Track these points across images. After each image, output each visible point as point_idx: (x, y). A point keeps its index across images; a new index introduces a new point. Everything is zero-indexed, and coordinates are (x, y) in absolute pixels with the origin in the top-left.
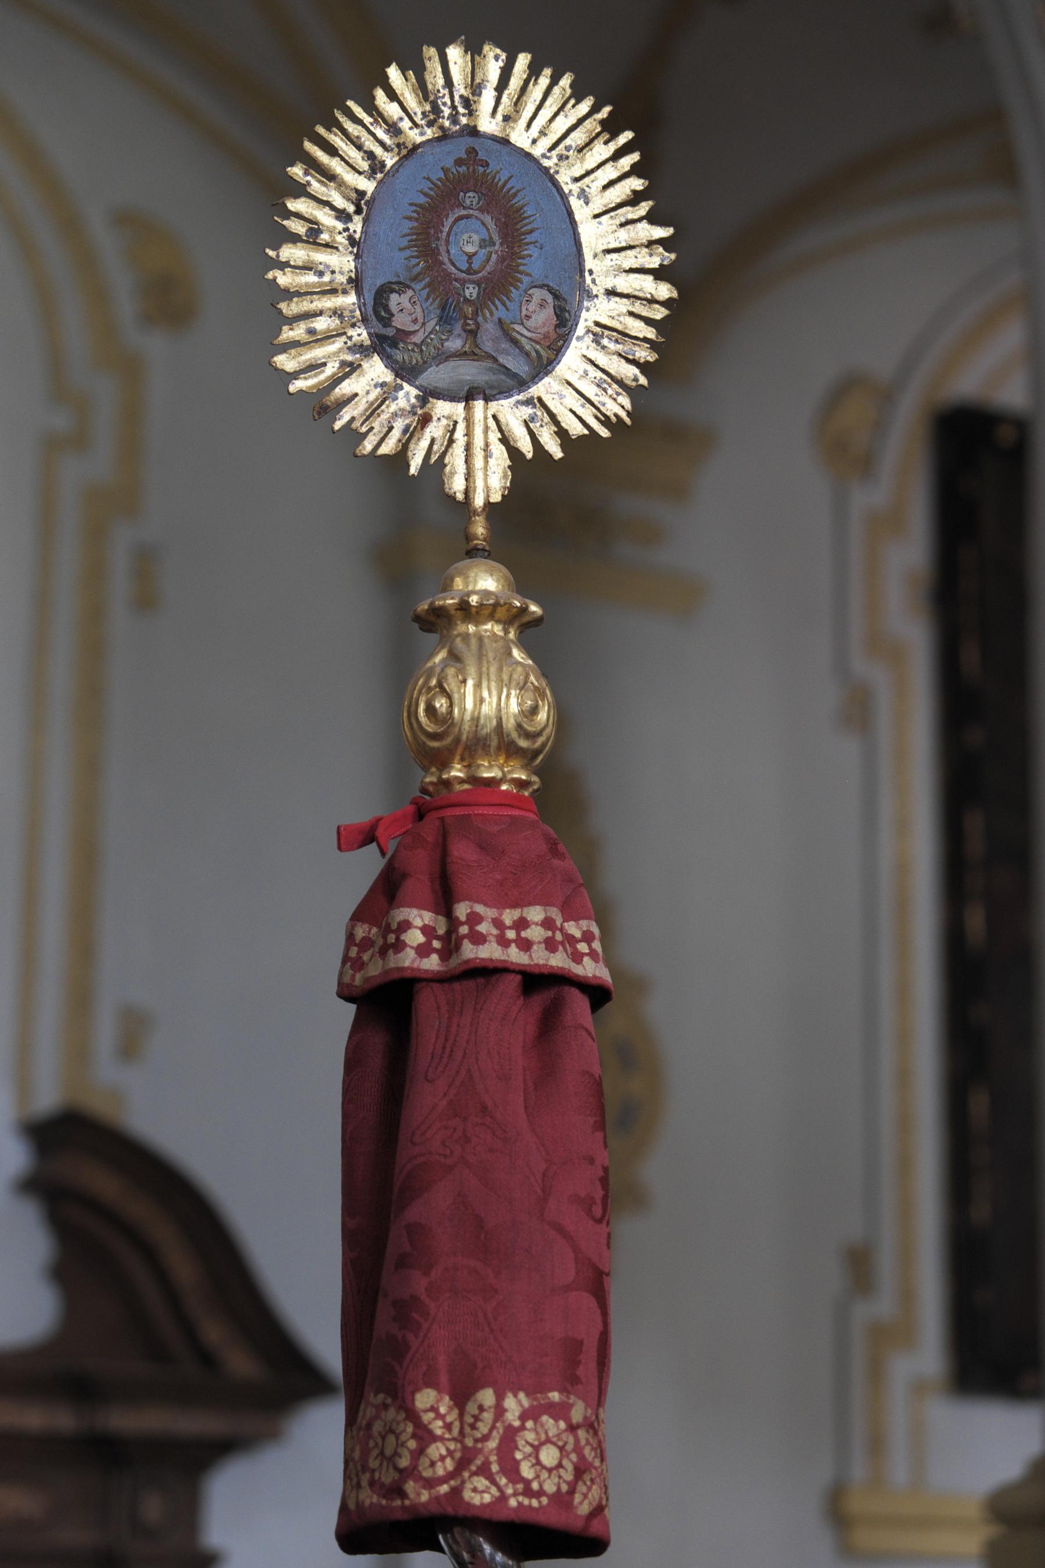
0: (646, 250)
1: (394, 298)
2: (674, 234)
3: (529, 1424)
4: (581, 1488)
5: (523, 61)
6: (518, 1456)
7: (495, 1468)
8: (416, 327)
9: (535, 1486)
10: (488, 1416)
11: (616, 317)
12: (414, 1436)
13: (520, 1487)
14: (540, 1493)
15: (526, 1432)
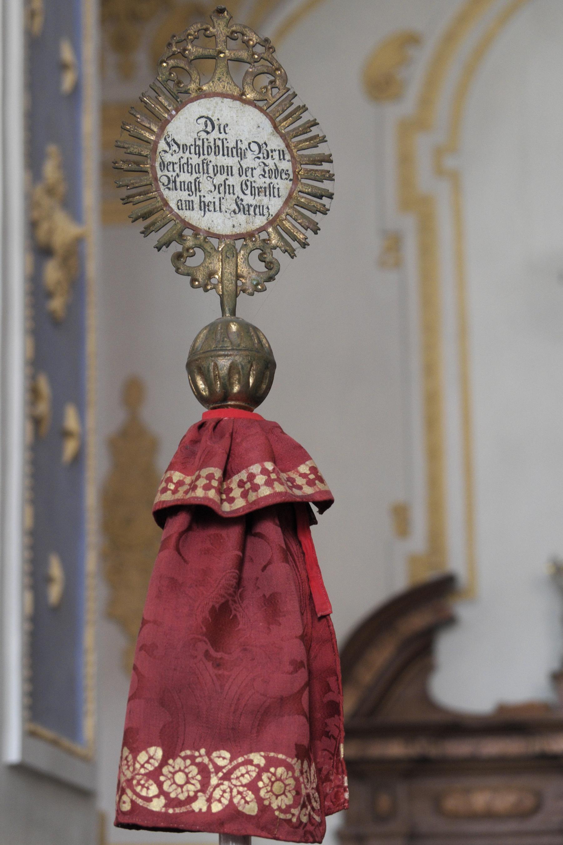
0: (154, 757)
6: (199, 777)
9: (188, 762)
11: (288, 777)
12: (259, 789)
14: (184, 758)
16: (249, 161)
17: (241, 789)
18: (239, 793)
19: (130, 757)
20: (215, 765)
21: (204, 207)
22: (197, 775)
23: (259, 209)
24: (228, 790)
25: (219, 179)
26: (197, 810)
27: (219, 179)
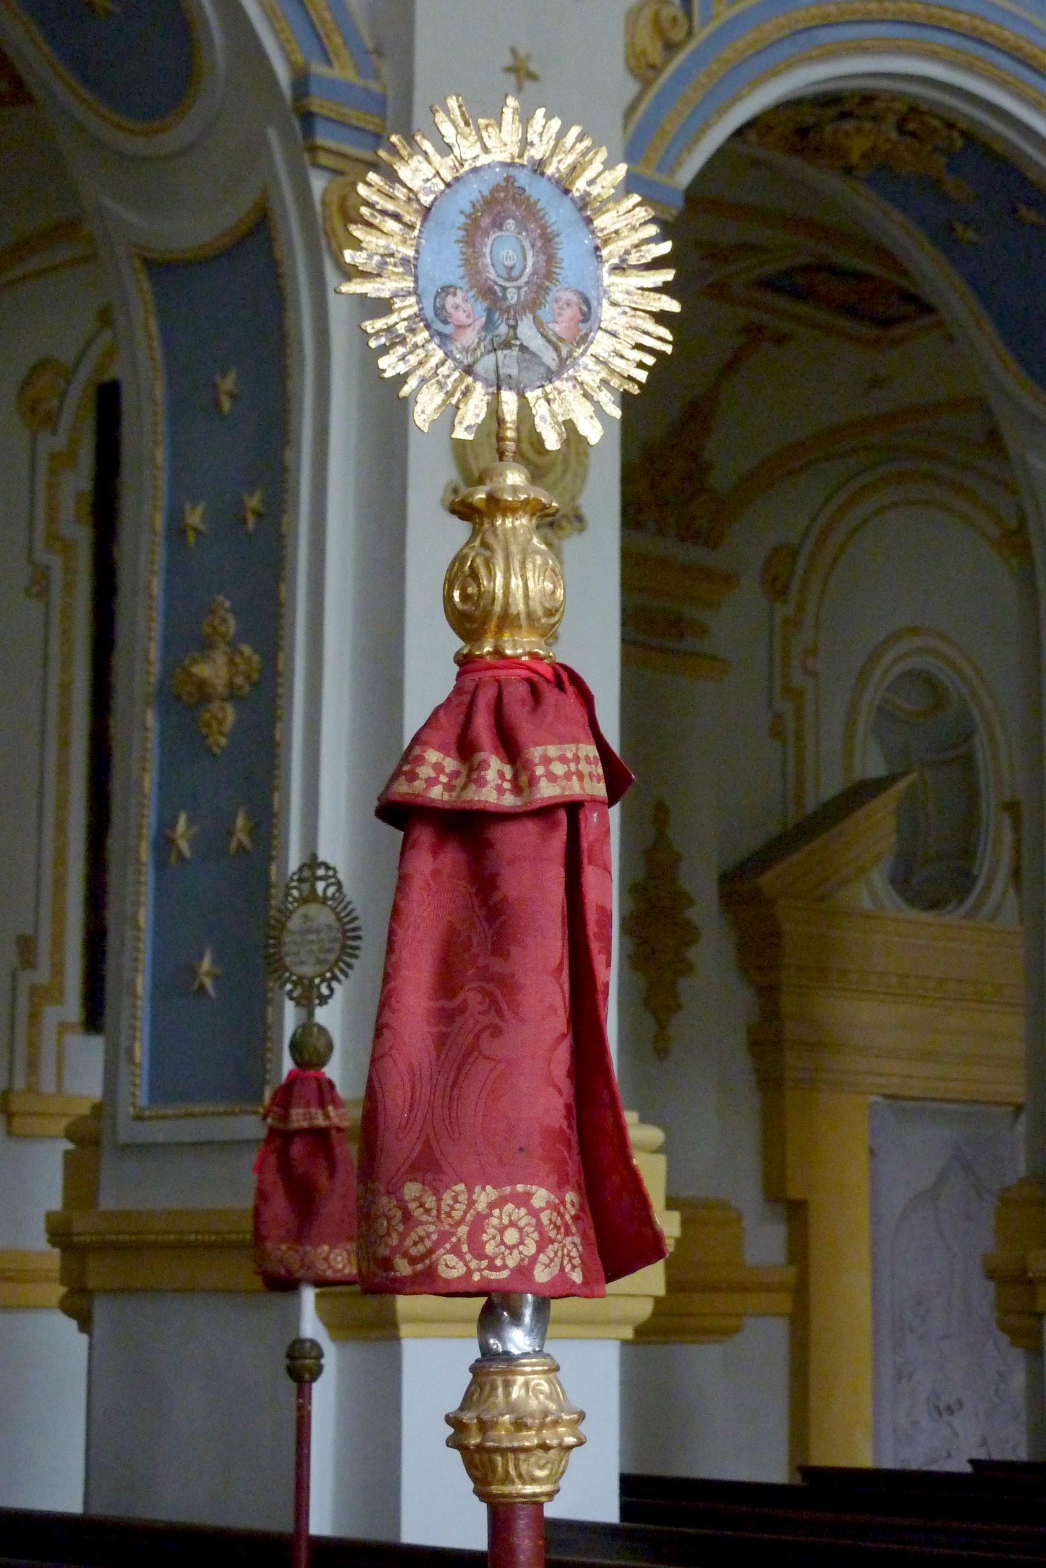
0: (544, 1267)
1: (450, 301)
2: (634, 395)
3: (496, 1212)
4: (542, 1258)
5: (575, 131)
7: (465, 1248)
8: (470, 321)
9: (498, 1262)
10: (460, 1207)
13: (484, 1263)
15: (492, 1218)
16: (323, 936)
17: (425, 1218)
18: (428, 1211)
19: (568, 1268)
20: (460, 1256)
21: (302, 963)
22: (487, 1242)
23: (325, 961)
24: (443, 1216)
25: (308, 948)
26: (488, 1188)
27: (308, 948)
